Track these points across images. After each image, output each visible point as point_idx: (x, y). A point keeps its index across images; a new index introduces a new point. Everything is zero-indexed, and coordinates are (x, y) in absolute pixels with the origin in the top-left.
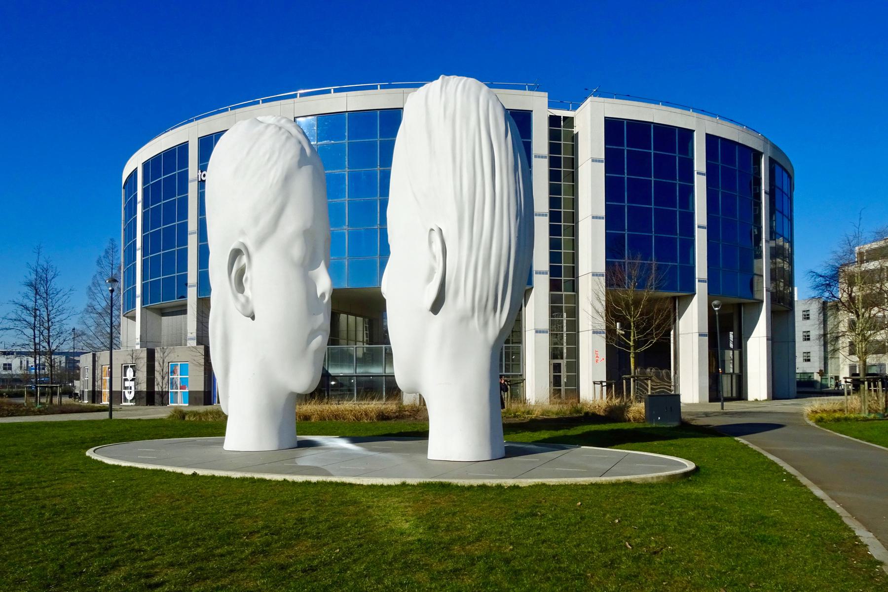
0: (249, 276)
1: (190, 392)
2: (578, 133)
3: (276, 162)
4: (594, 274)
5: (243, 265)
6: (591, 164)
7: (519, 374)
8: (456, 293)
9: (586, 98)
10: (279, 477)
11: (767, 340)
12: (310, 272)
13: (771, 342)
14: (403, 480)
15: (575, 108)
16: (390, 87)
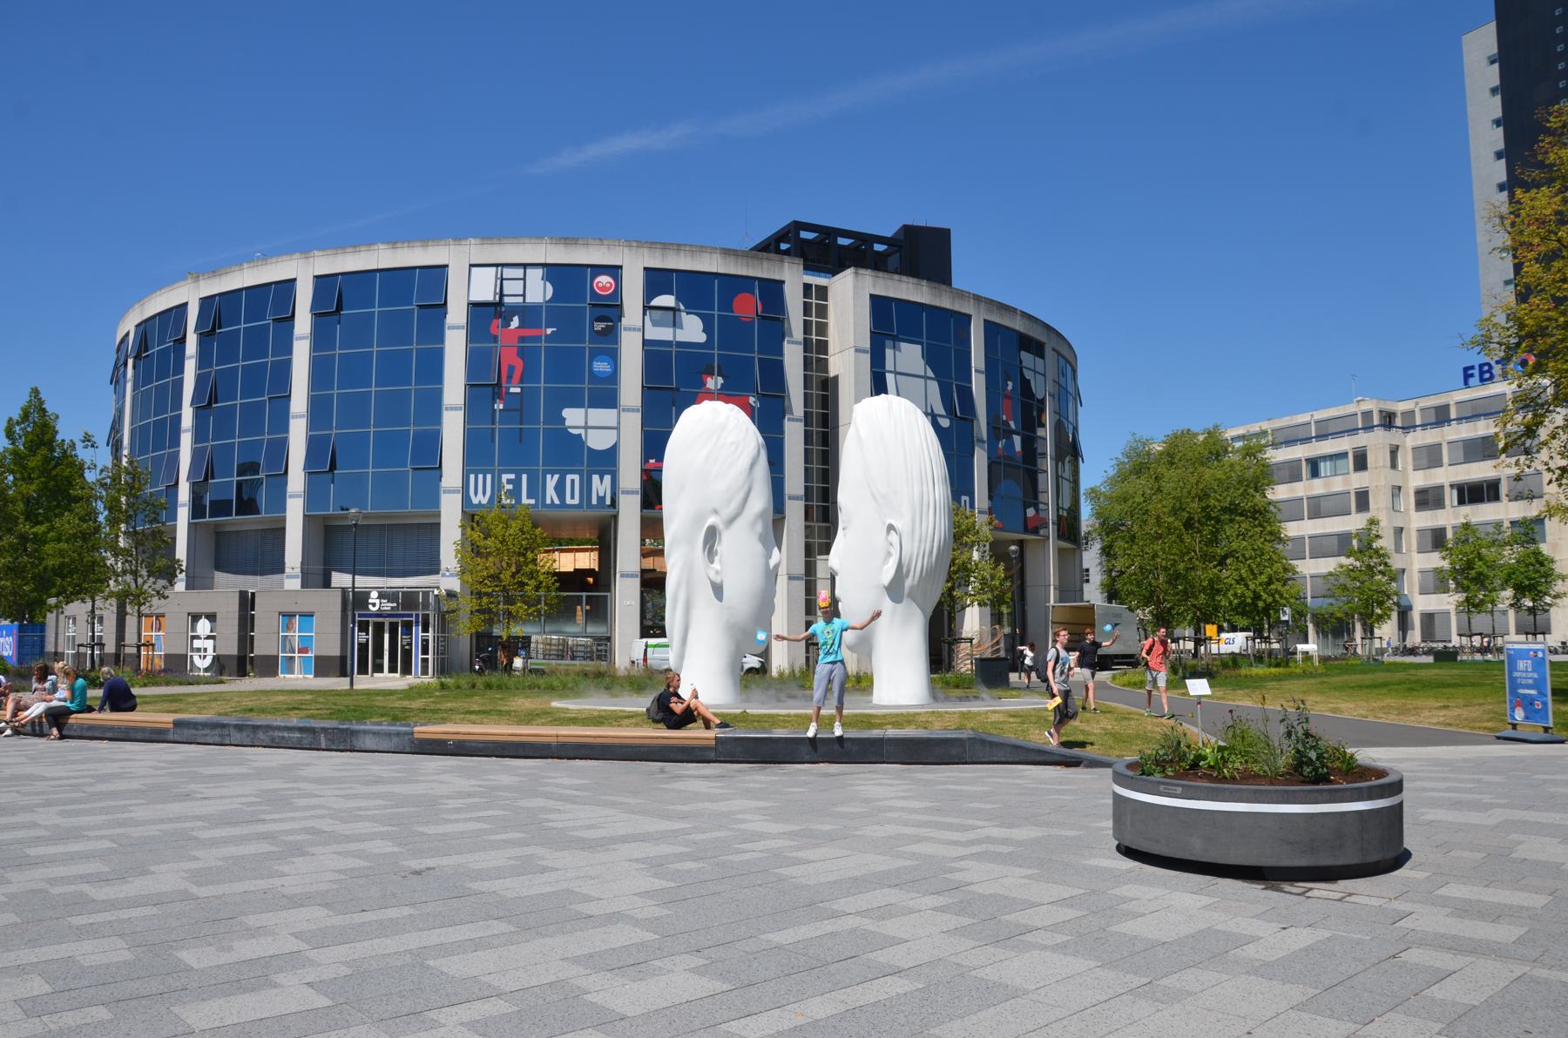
1: (317, 658)
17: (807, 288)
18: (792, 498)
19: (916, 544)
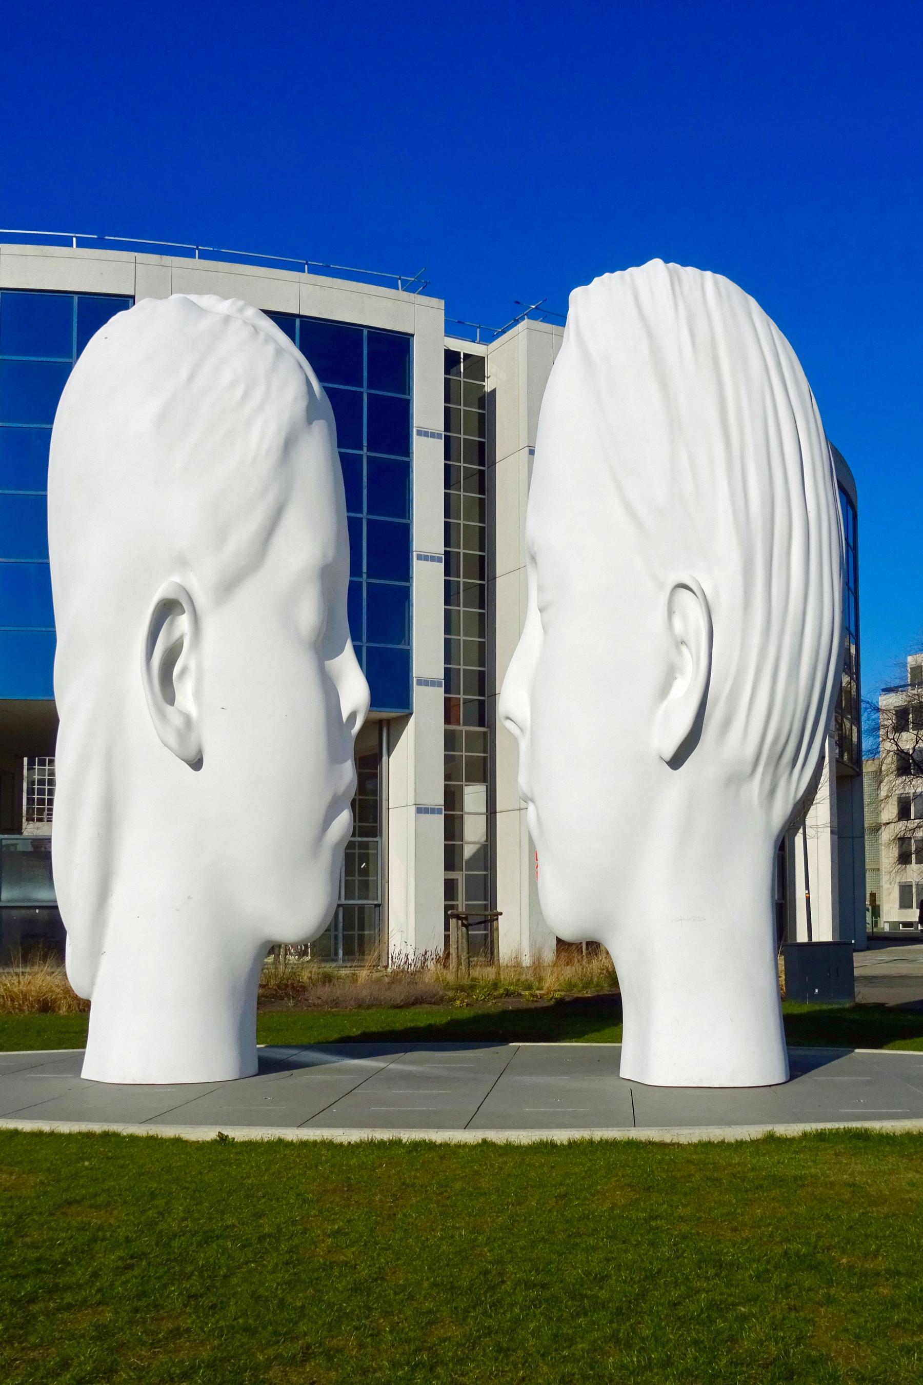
0: (192, 665)
2: (494, 390)
3: (260, 408)
5: (179, 639)
6: (528, 458)
7: (375, 902)
9: (517, 322)
10: (471, 1137)
11: (832, 833)
12: (328, 663)
13: (836, 837)
14: (768, 1128)
15: (488, 338)
16: (100, 245)
17: (451, 358)
18: (422, 682)
19: (755, 640)
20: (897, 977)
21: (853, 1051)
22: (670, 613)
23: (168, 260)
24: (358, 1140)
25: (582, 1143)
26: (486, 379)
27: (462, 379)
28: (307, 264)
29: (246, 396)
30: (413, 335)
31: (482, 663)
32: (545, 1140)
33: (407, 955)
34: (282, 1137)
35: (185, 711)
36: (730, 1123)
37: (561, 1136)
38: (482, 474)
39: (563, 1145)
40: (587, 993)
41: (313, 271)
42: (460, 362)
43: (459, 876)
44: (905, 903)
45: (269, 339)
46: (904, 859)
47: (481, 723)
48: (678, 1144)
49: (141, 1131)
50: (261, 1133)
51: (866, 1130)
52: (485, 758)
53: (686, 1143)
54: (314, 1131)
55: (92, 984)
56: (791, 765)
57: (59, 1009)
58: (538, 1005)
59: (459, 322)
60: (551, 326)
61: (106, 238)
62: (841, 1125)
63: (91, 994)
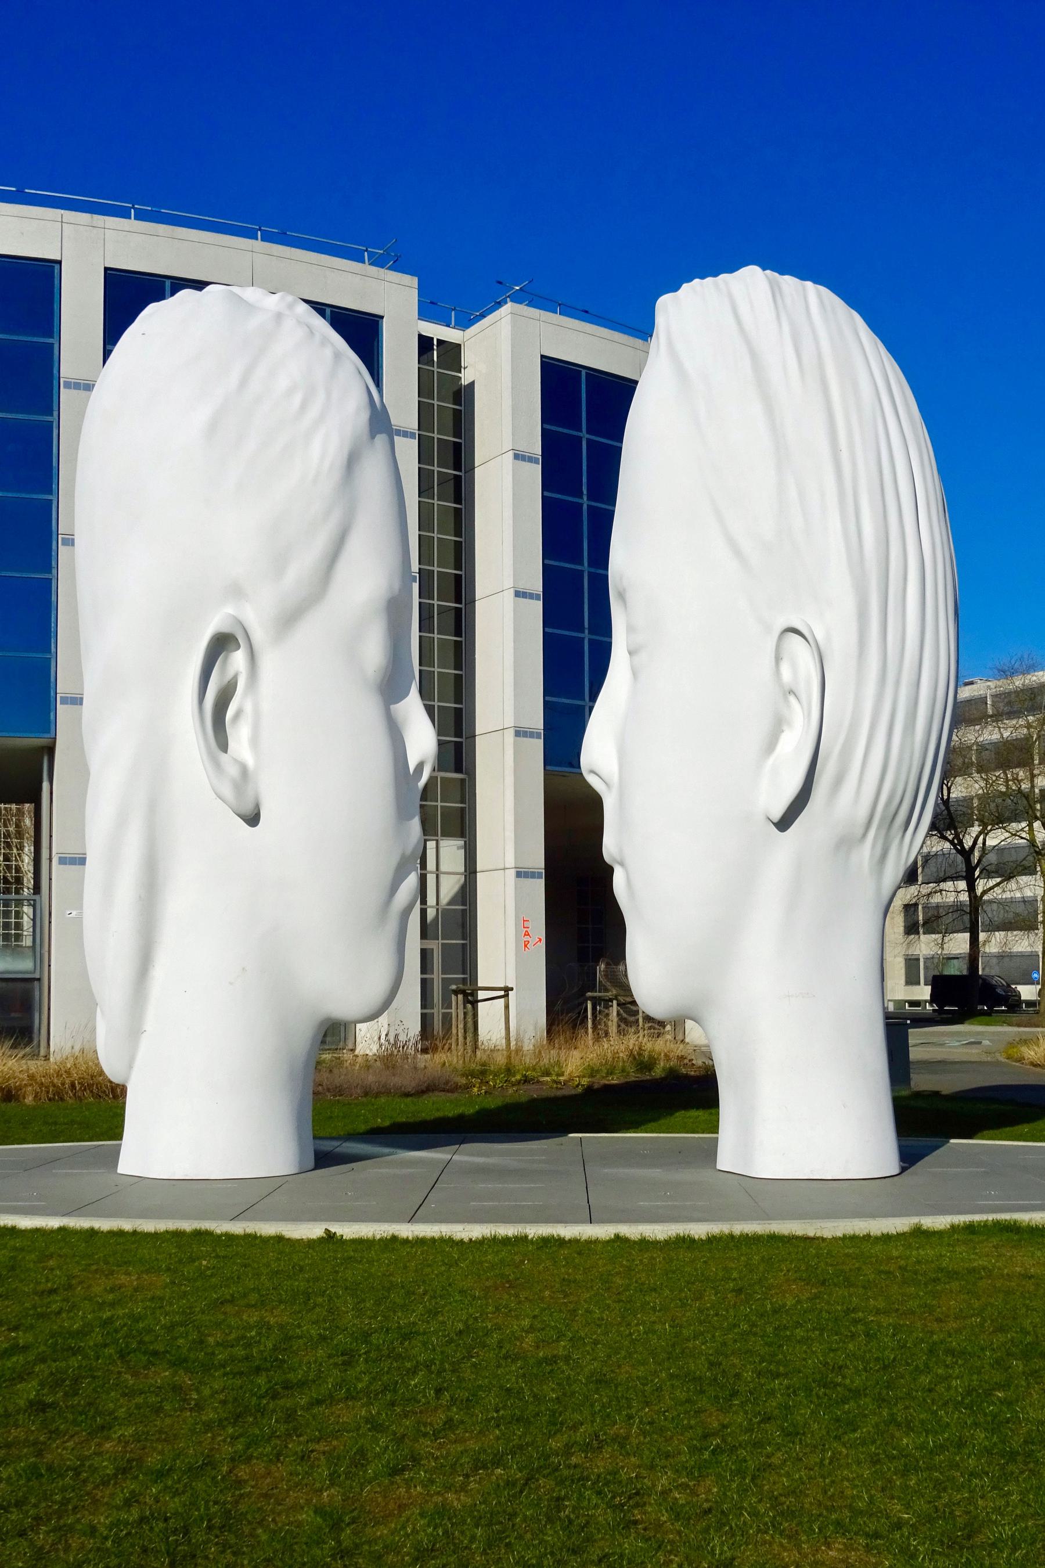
0: (248, 707)
2: (473, 383)
4: (520, 733)
8: (839, 781)
9: (499, 304)
12: (392, 707)
14: (914, 1220)
15: (465, 323)
17: (425, 344)
20: (934, 1062)
21: (948, 1142)
22: (778, 659)
23: (99, 220)
24: (480, 1237)
25: (721, 1238)
26: (462, 370)
27: (435, 369)
28: (260, 230)
29: (304, 406)
30: (382, 317)
31: (458, 699)
32: (682, 1235)
33: (397, 1036)
34: (396, 1234)
35: (239, 759)
36: (873, 1216)
37: (699, 1230)
38: (457, 479)
39: (702, 1240)
40: (613, 1079)
41: (267, 238)
42: (433, 349)
43: (435, 946)
44: (912, 980)
45: (325, 341)
46: (911, 929)
47: (458, 769)
48: (823, 1239)
49: (237, 1228)
50: (372, 1230)
51: (1015, 1222)
52: (463, 809)
53: (830, 1237)
54: (431, 1227)
55: (130, 1067)
56: (902, 831)
57: (24, 1098)
58: (559, 1093)
59: (432, 303)
60: (538, 311)
61: (27, 191)
62: (990, 1217)
63: (127, 1079)
